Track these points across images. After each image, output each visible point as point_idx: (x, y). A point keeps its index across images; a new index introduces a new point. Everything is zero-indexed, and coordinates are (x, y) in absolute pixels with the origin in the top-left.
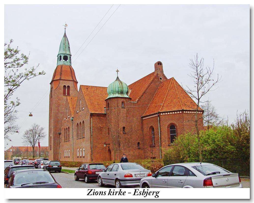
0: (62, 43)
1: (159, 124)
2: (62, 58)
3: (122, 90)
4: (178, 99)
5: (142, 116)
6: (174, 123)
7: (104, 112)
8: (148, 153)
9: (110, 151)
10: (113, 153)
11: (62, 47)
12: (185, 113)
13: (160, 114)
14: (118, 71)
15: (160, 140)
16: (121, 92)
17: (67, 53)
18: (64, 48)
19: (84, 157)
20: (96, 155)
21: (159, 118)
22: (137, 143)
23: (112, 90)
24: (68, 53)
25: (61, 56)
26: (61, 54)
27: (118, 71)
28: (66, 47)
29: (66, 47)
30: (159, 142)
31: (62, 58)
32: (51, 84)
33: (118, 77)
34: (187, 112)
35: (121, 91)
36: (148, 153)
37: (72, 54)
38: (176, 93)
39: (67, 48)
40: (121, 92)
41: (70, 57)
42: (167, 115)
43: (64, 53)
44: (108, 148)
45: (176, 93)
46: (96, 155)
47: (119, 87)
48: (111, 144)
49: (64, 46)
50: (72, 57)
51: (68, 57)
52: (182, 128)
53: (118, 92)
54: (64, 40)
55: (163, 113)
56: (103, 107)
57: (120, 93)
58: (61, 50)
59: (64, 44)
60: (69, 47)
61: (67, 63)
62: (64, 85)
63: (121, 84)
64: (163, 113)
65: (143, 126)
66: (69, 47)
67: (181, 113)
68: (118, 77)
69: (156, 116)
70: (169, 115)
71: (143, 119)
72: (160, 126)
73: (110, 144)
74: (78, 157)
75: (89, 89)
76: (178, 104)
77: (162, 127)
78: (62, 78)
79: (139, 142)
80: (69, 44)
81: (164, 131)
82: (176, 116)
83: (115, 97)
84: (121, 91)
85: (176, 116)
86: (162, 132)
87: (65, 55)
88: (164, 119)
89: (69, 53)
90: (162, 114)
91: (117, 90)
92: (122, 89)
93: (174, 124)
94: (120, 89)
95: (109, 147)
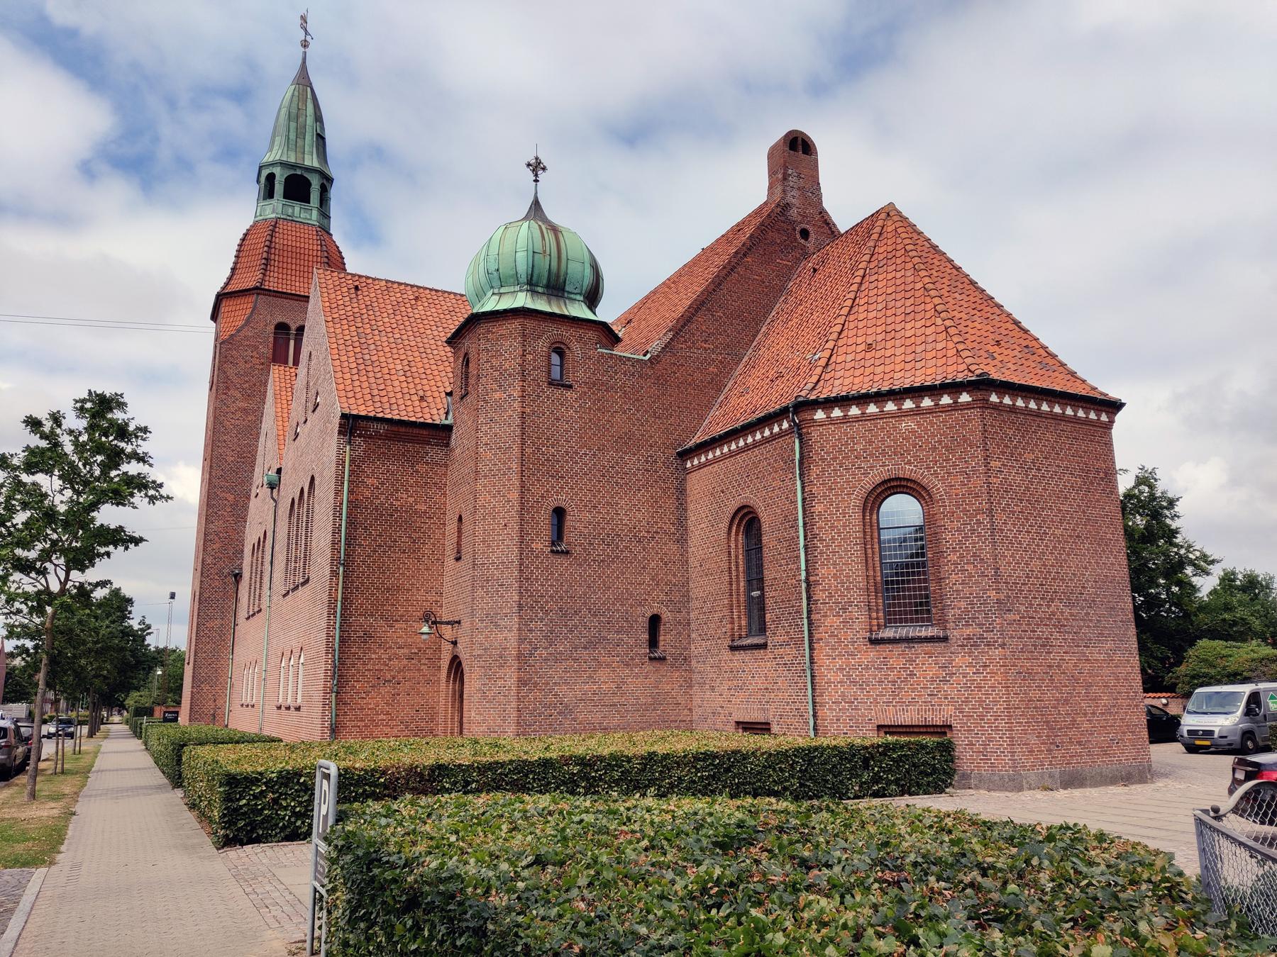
0: (284, 111)
1: (798, 483)
2: (279, 188)
3: (558, 275)
4: (939, 321)
5: (679, 445)
6: (913, 476)
7: (439, 419)
8: (712, 688)
9: (460, 663)
10: (472, 683)
11: (282, 130)
12: (995, 407)
13: (806, 416)
14: (537, 167)
15: (809, 598)
16: (548, 286)
17: (307, 163)
18: (292, 136)
19: (298, 709)
20: (367, 693)
21: (797, 441)
22: (643, 622)
23: (493, 268)
24: (312, 161)
25: (271, 177)
26: (272, 164)
27: (537, 167)
28: (301, 133)
29: (301, 133)
30: (799, 612)
31: (279, 188)
32: (214, 317)
33: (536, 204)
34: (1014, 398)
35: (553, 277)
36: (712, 688)
37: (333, 171)
38: (919, 286)
39: (308, 137)
40: (548, 286)
41: (324, 191)
42: (856, 419)
43: (292, 160)
44: (450, 647)
45: (919, 286)
46: (367, 693)
47: (538, 248)
48: (466, 624)
49: (293, 125)
50: (334, 192)
51: (309, 184)
52: (978, 511)
53: (531, 285)
54: (295, 99)
55: (828, 403)
56: (442, 389)
57: (540, 290)
58: (276, 148)
59: (293, 115)
60: (318, 135)
61: (307, 214)
62: (280, 319)
63: (550, 236)
64: (828, 403)
65: (686, 510)
66: (318, 135)
67: (967, 406)
68: (536, 204)
69: (782, 434)
70: (873, 418)
71: (689, 465)
72: (804, 500)
73: (459, 622)
74: (279, 708)
75: (367, 296)
76: (940, 346)
77: (819, 508)
78: (271, 285)
79: (655, 611)
80: (318, 118)
81: (839, 533)
82: (932, 424)
83: (505, 311)
84: (553, 277)
85: (932, 424)
86: (821, 540)
87: (292, 172)
88: (834, 446)
89: (316, 164)
90: (820, 415)
91: (522, 268)
92: (554, 264)
93: (915, 482)
94: (543, 264)
95: (455, 643)
